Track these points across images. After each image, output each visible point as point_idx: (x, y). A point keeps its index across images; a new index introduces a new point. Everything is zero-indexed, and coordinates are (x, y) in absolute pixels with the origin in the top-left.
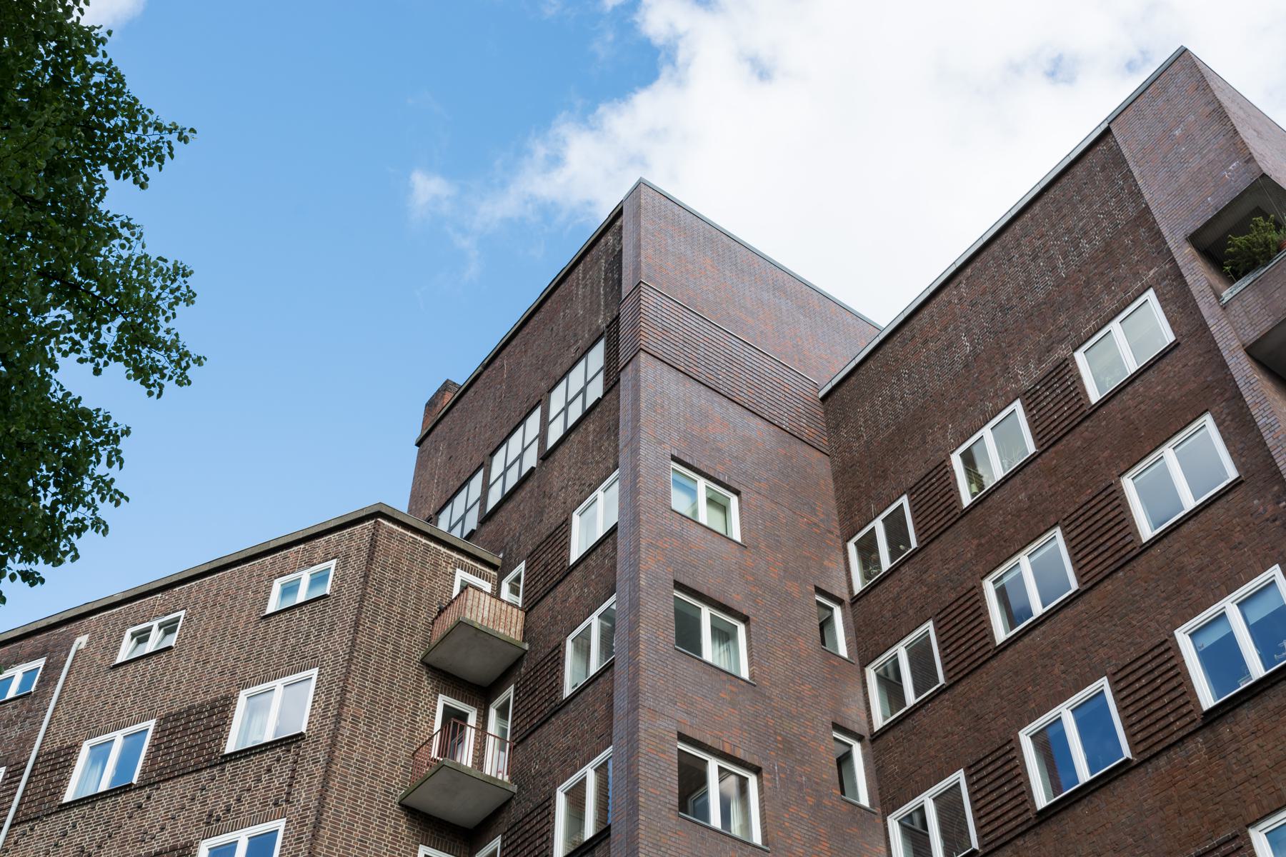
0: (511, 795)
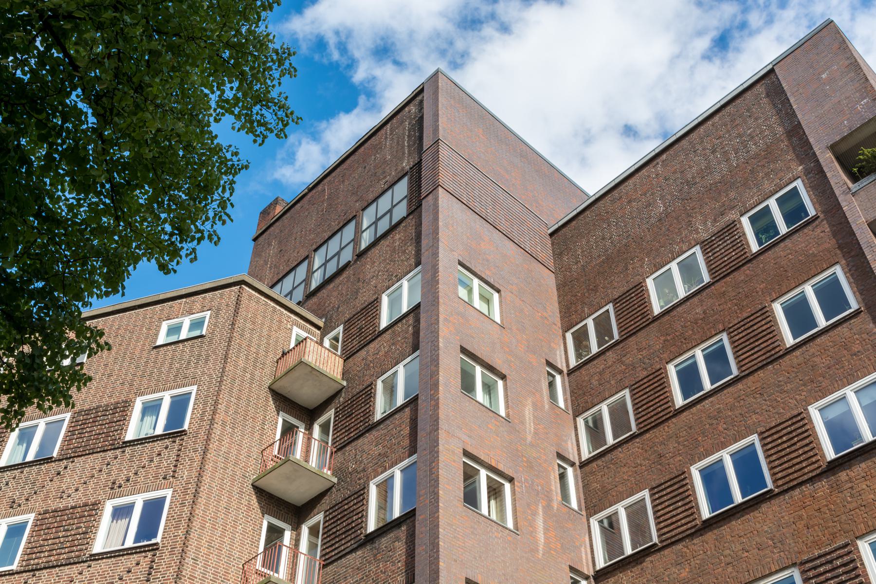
0: (332, 484)
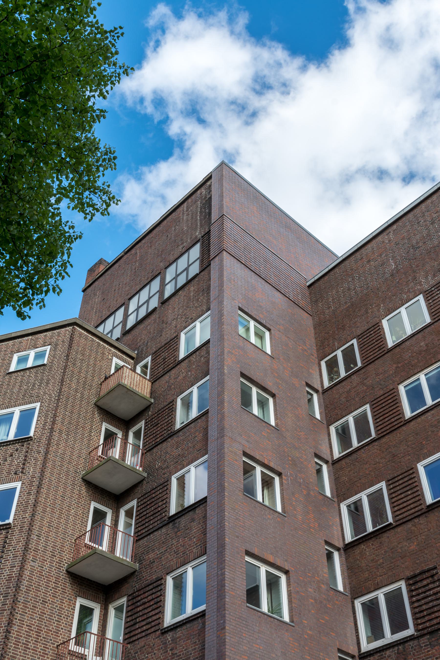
0: (143, 478)
